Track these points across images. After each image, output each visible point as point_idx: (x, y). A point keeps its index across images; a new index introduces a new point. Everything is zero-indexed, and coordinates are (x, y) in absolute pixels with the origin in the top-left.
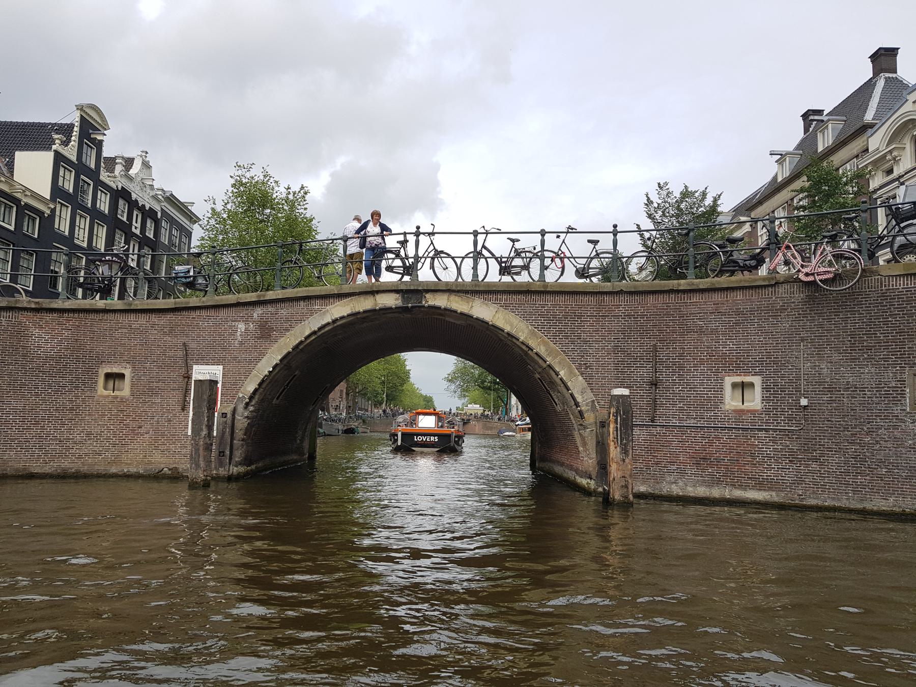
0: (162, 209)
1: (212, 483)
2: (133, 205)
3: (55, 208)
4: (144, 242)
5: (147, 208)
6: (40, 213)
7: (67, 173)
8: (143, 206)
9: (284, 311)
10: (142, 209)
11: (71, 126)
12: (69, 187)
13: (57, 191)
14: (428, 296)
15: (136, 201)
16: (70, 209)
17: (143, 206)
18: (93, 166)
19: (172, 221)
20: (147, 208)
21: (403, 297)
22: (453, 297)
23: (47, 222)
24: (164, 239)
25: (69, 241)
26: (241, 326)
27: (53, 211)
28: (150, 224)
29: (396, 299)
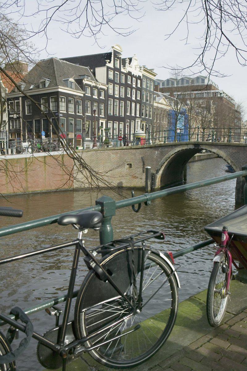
0: (143, 75)
1: (39, 140)
2: (132, 76)
3: (108, 86)
4: (137, 89)
5: (137, 76)
6: (103, 89)
7: (111, 72)
8: (136, 76)
9: (166, 149)
10: (136, 77)
11: (111, 53)
12: (111, 77)
13: (109, 81)
14: (201, 145)
15: (134, 75)
16: (113, 85)
17: (136, 76)
18: (118, 67)
19: (147, 78)
20: (137, 76)
21: (194, 146)
22: (207, 146)
23: (106, 92)
24: (144, 86)
25: (113, 97)
26: (157, 152)
27: (108, 88)
28: (139, 81)
29: (193, 146)
